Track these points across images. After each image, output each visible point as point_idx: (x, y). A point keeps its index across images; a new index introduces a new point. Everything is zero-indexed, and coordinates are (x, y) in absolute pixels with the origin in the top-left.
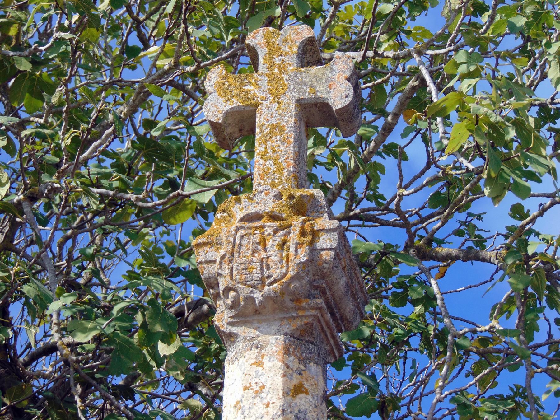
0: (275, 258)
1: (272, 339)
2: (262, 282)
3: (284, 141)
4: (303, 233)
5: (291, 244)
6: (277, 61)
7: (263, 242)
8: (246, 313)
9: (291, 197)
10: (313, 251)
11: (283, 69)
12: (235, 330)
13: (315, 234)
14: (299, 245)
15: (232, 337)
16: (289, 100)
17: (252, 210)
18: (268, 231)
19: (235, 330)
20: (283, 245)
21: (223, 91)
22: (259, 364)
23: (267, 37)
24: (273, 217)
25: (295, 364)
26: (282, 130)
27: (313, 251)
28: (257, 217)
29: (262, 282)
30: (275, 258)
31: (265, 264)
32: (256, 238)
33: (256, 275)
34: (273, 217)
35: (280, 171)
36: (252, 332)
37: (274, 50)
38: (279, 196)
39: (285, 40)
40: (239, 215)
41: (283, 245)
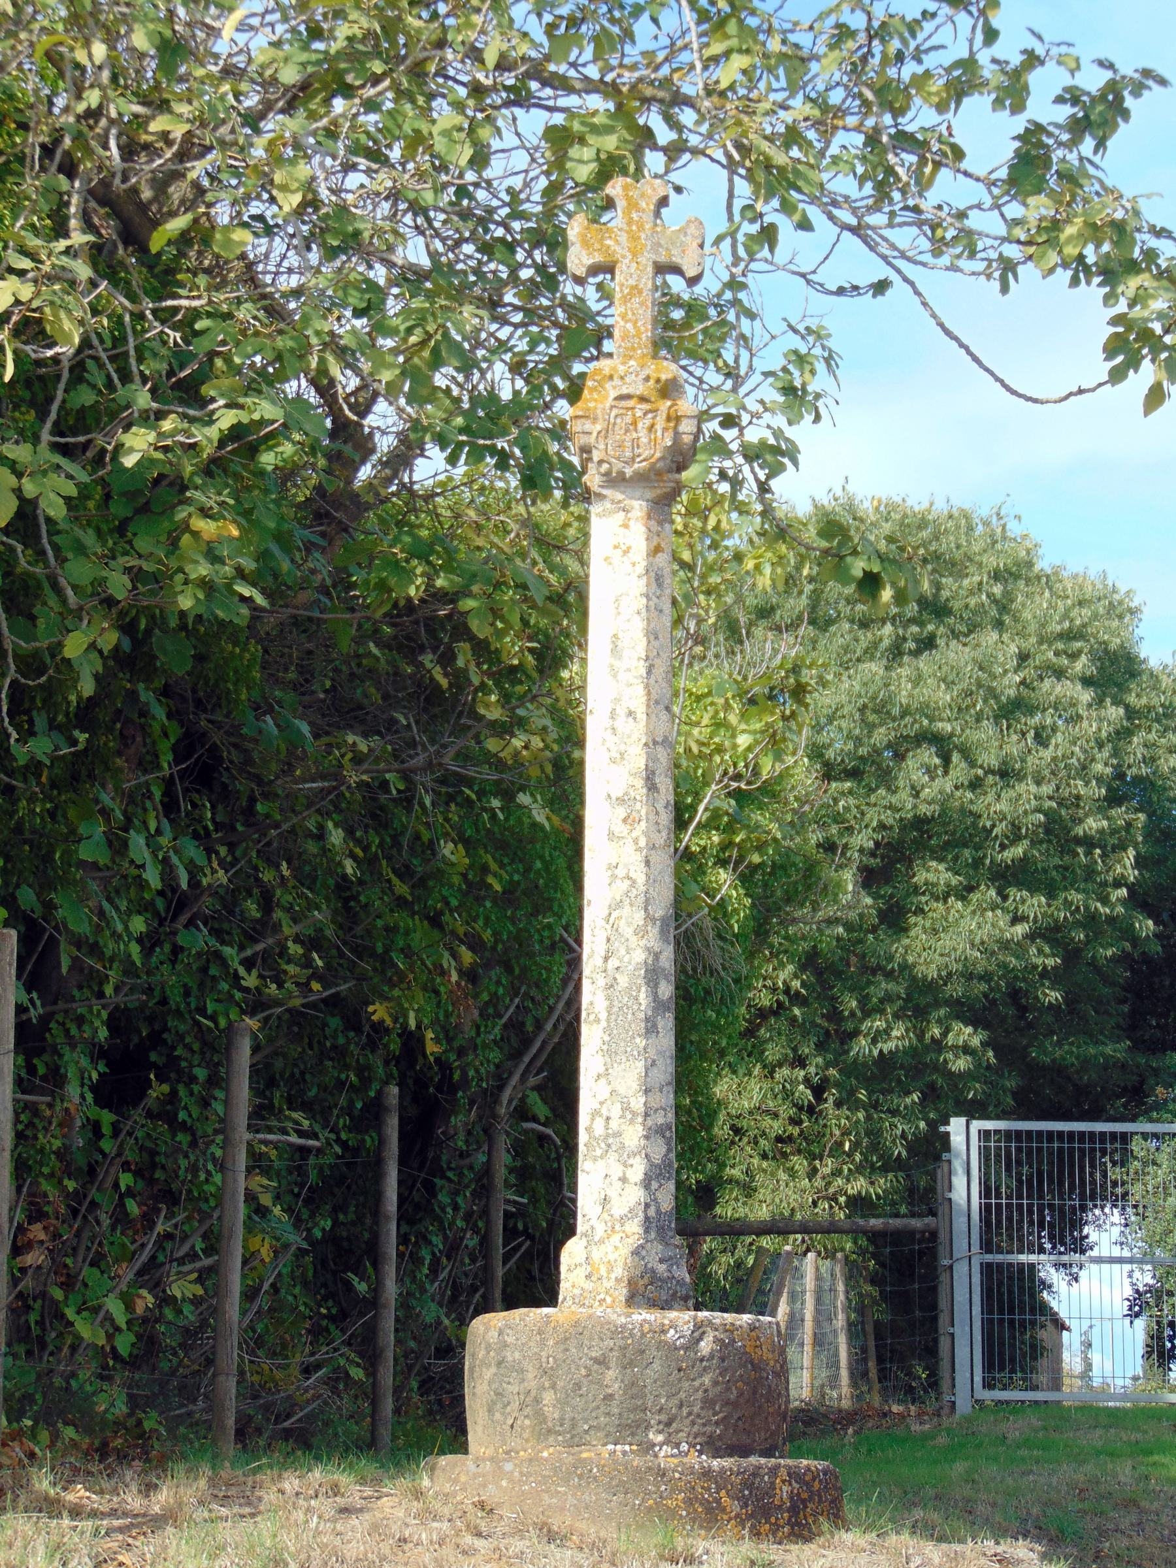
0: (644, 440)
1: (637, 504)
2: (633, 459)
3: (642, 304)
4: (669, 419)
5: (659, 427)
6: (634, 216)
7: (634, 423)
8: (615, 480)
9: (658, 381)
10: (677, 434)
11: (641, 227)
12: (604, 492)
13: (678, 419)
14: (665, 429)
15: (600, 496)
16: (647, 260)
17: (625, 391)
18: (639, 414)
19: (604, 492)
20: (651, 428)
21: (586, 244)
22: (625, 526)
23: (625, 188)
24: (643, 399)
25: (655, 527)
26: (640, 292)
27: (677, 434)
28: (628, 397)
29: (633, 459)
30: (644, 440)
31: (636, 443)
32: (628, 419)
33: (628, 454)
34: (643, 399)
35: (638, 335)
36: (619, 496)
37: (632, 205)
38: (647, 379)
39: (642, 195)
40: (613, 394)
41: (651, 428)
